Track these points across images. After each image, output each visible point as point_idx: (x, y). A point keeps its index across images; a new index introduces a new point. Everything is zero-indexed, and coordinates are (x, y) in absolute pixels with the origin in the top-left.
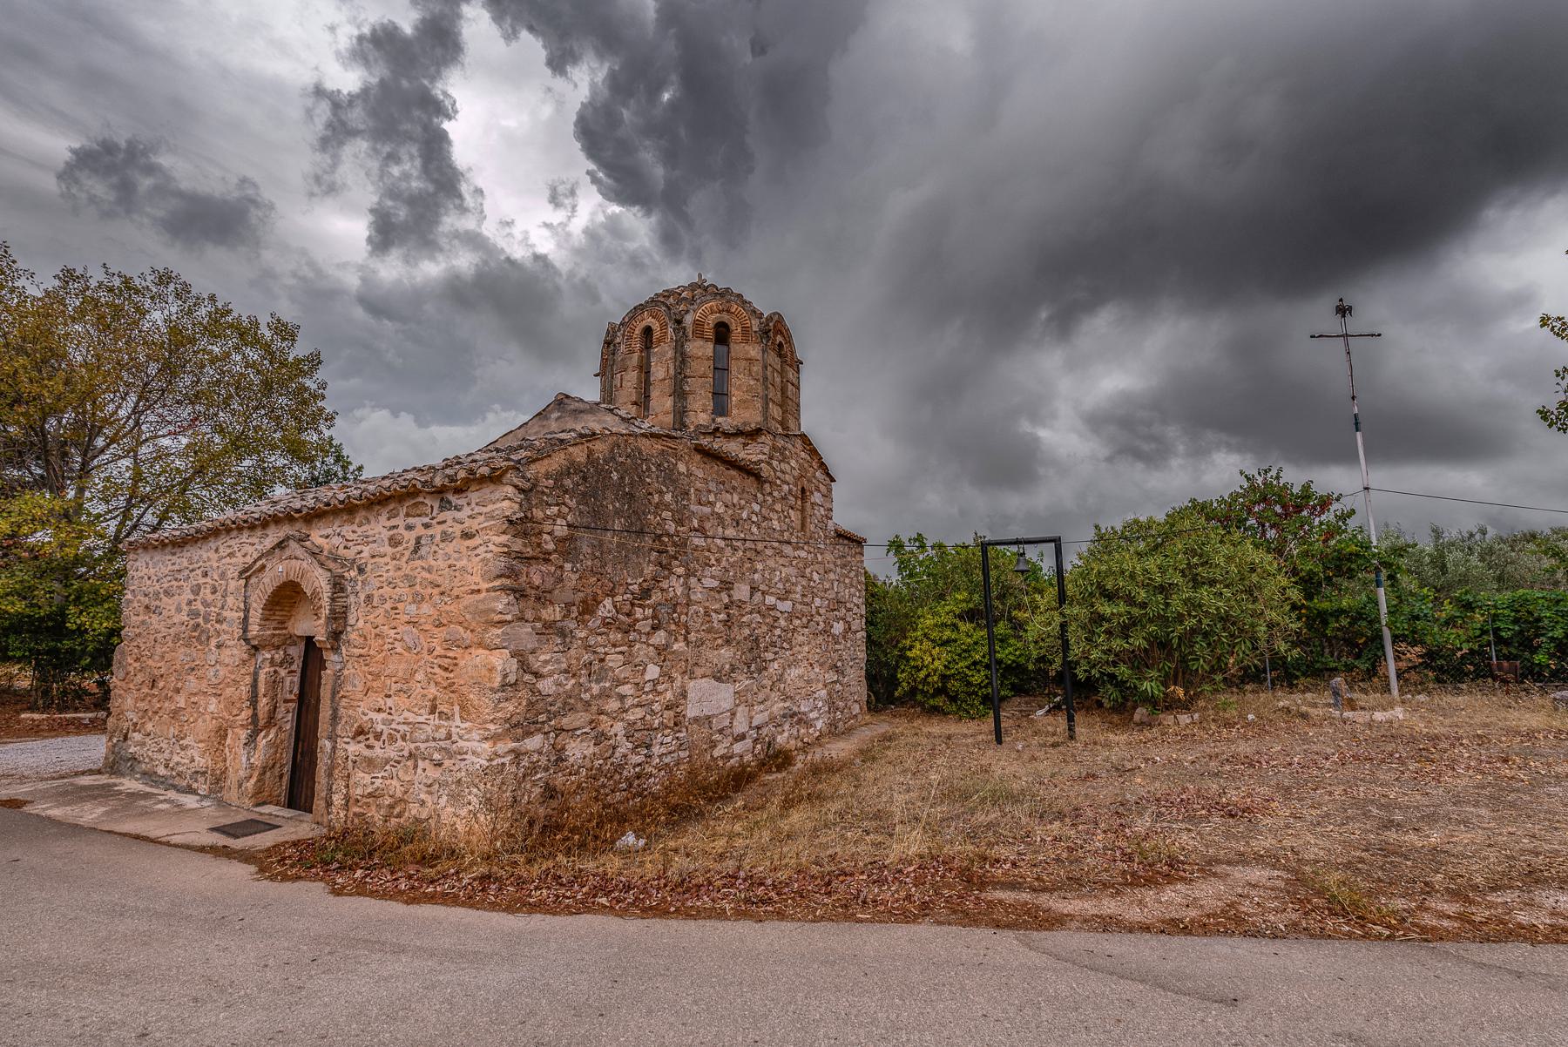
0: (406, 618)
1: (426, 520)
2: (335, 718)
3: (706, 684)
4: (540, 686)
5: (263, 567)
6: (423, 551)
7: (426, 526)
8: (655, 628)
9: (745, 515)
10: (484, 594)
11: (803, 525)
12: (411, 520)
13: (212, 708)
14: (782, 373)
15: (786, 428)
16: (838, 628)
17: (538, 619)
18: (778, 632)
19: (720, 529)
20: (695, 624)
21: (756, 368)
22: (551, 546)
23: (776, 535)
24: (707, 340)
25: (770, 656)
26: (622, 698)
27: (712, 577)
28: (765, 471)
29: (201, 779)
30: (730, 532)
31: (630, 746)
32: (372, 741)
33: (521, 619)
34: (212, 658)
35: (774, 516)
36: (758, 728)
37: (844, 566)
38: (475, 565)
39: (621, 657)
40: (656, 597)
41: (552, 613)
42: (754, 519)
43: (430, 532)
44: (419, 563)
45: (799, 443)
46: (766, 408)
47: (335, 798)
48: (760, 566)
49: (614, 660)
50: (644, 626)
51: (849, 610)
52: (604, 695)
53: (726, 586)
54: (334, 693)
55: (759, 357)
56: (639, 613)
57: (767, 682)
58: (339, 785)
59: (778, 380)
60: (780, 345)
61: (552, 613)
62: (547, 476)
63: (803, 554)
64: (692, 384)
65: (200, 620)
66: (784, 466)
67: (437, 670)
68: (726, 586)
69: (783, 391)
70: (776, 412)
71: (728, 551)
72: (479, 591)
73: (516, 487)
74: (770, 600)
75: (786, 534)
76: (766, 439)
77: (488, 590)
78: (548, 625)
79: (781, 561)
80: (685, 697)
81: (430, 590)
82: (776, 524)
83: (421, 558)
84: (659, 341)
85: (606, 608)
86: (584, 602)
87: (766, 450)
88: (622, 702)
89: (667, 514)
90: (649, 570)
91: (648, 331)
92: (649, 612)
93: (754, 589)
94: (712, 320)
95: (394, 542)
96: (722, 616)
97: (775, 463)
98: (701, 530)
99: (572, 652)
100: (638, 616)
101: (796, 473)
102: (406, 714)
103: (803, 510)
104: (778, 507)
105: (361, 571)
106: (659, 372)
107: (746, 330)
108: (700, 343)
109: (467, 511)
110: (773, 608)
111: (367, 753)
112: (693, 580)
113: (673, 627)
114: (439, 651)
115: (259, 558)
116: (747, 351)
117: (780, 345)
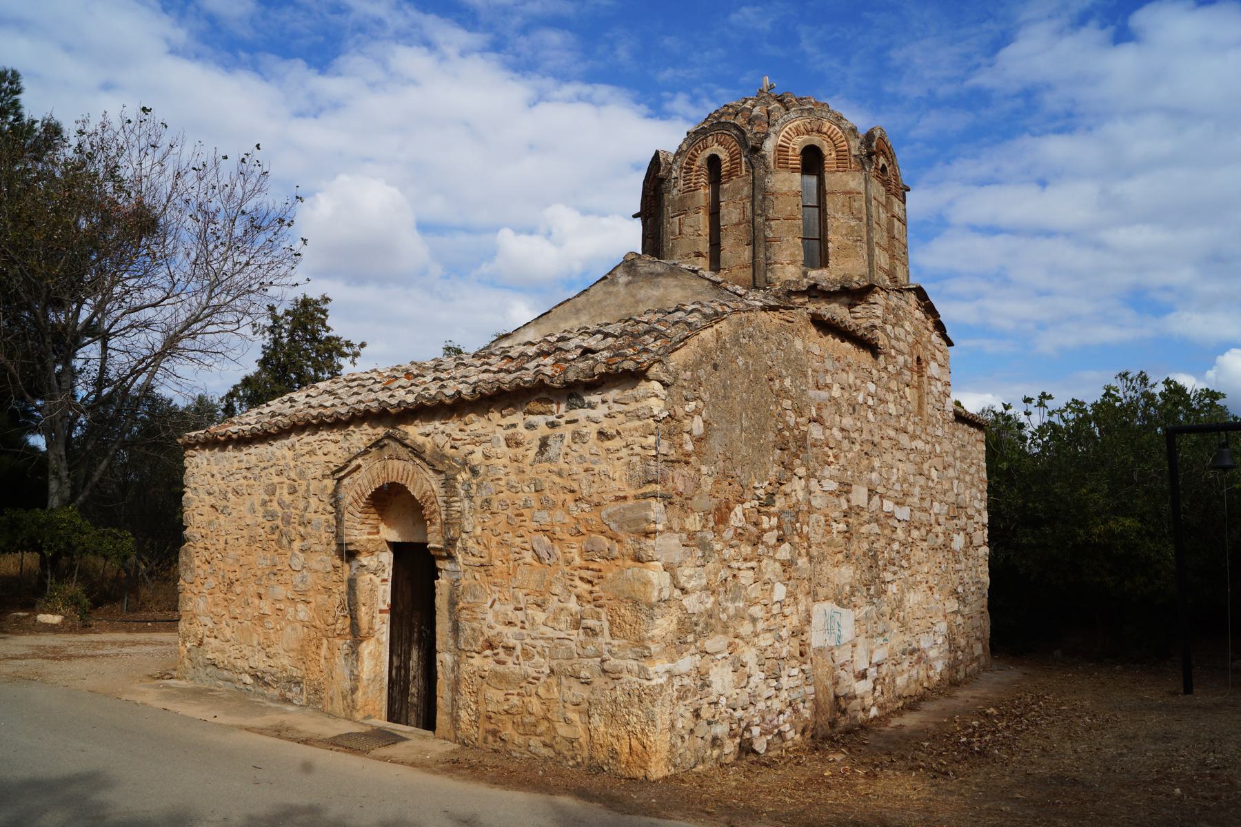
0: (535, 525)
1: (552, 418)
2: (456, 629)
3: (829, 606)
4: (685, 602)
5: (359, 467)
6: (552, 451)
7: (552, 425)
8: (780, 540)
9: (860, 399)
10: (631, 502)
11: (920, 406)
12: (531, 418)
13: (301, 615)
14: (888, 206)
15: (894, 279)
16: (959, 541)
17: (683, 529)
18: (896, 546)
19: (837, 418)
20: (816, 538)
21: (860, 204)
22: (689, 447)
23: (893, 422)
24: (794, 170)
25: (888, 576)
26: (754, 620)
27: (832, 478)
28: (882, 341)
29: (296, 690)
30: (847, 421)
31: (763, 675)
32: (502, 655)
33: (670, 529)
34: (297, 563)
35: (890, 397)
36: (878, 665)
37: (963, 459)
38: (618, 471)
39: (751, 573)
40: (780, 503)
41: (693, 522)
42: (870, 402)
43: (558, 431)
44: (547, 465)
45: (912, 297)
46: (871, 255)
47: (462, 713)
48: (877, 463)
49: (746, 577)
50: (770, 538)
51: (970, 517)
52: (739, 616)
53: (845, 488)
54: (453, 603)
55: (862, 189)
56: (766, 522)
57: (886, 609)
58: (466, 698)
59: (883, 216)
60: (884, 169)
61: (693, 522)
62: (686, 367)
63: (919, 444)
64: (776, 228)
65: (279, 522)
66: (898, 330)
67: (578, 582)
68: (845, 488)
69: (890, 229)
70: (882, 259)
71: (846, 444)
72: (625, 498)
73: (661, 382)
74: (888, 506)
75: (903, 420)
76: (879, 298)
77: (636, 497)
78: (692, 535)
79: (899, 455)
80: (809, 622)
81: (562, 497)
82: (892, 408)
83: (549, 460)
84: (730, 174)
85: (737, 517)
86: (718, 509)
87: (879, 312)
88: (755, 625)
89: (787, 403)
90: (774, 471)
91: (714, 161)
92: (774, 521)
93: (872, 492)
94: (798, 143)
95: (513, 442)
96: (842, 527)
97: (889, 328)
98: (817, 420)
99: (710, 566)
100: (765, 526)
101: (910, 339)
102: (543, 629)
103: (919, 387)
104: (893, 385)
105: (474, 472)
106: (731, 214)
107: (842, 155)
108: (785, 175)
109: (601, 410)
110: (890, 515)
111: (500, 668)
112: (813, 482)
113: (797, 539)
114: (578, 561)
115: (355, 457)
116: (844, 181)
117: (884, 169)
